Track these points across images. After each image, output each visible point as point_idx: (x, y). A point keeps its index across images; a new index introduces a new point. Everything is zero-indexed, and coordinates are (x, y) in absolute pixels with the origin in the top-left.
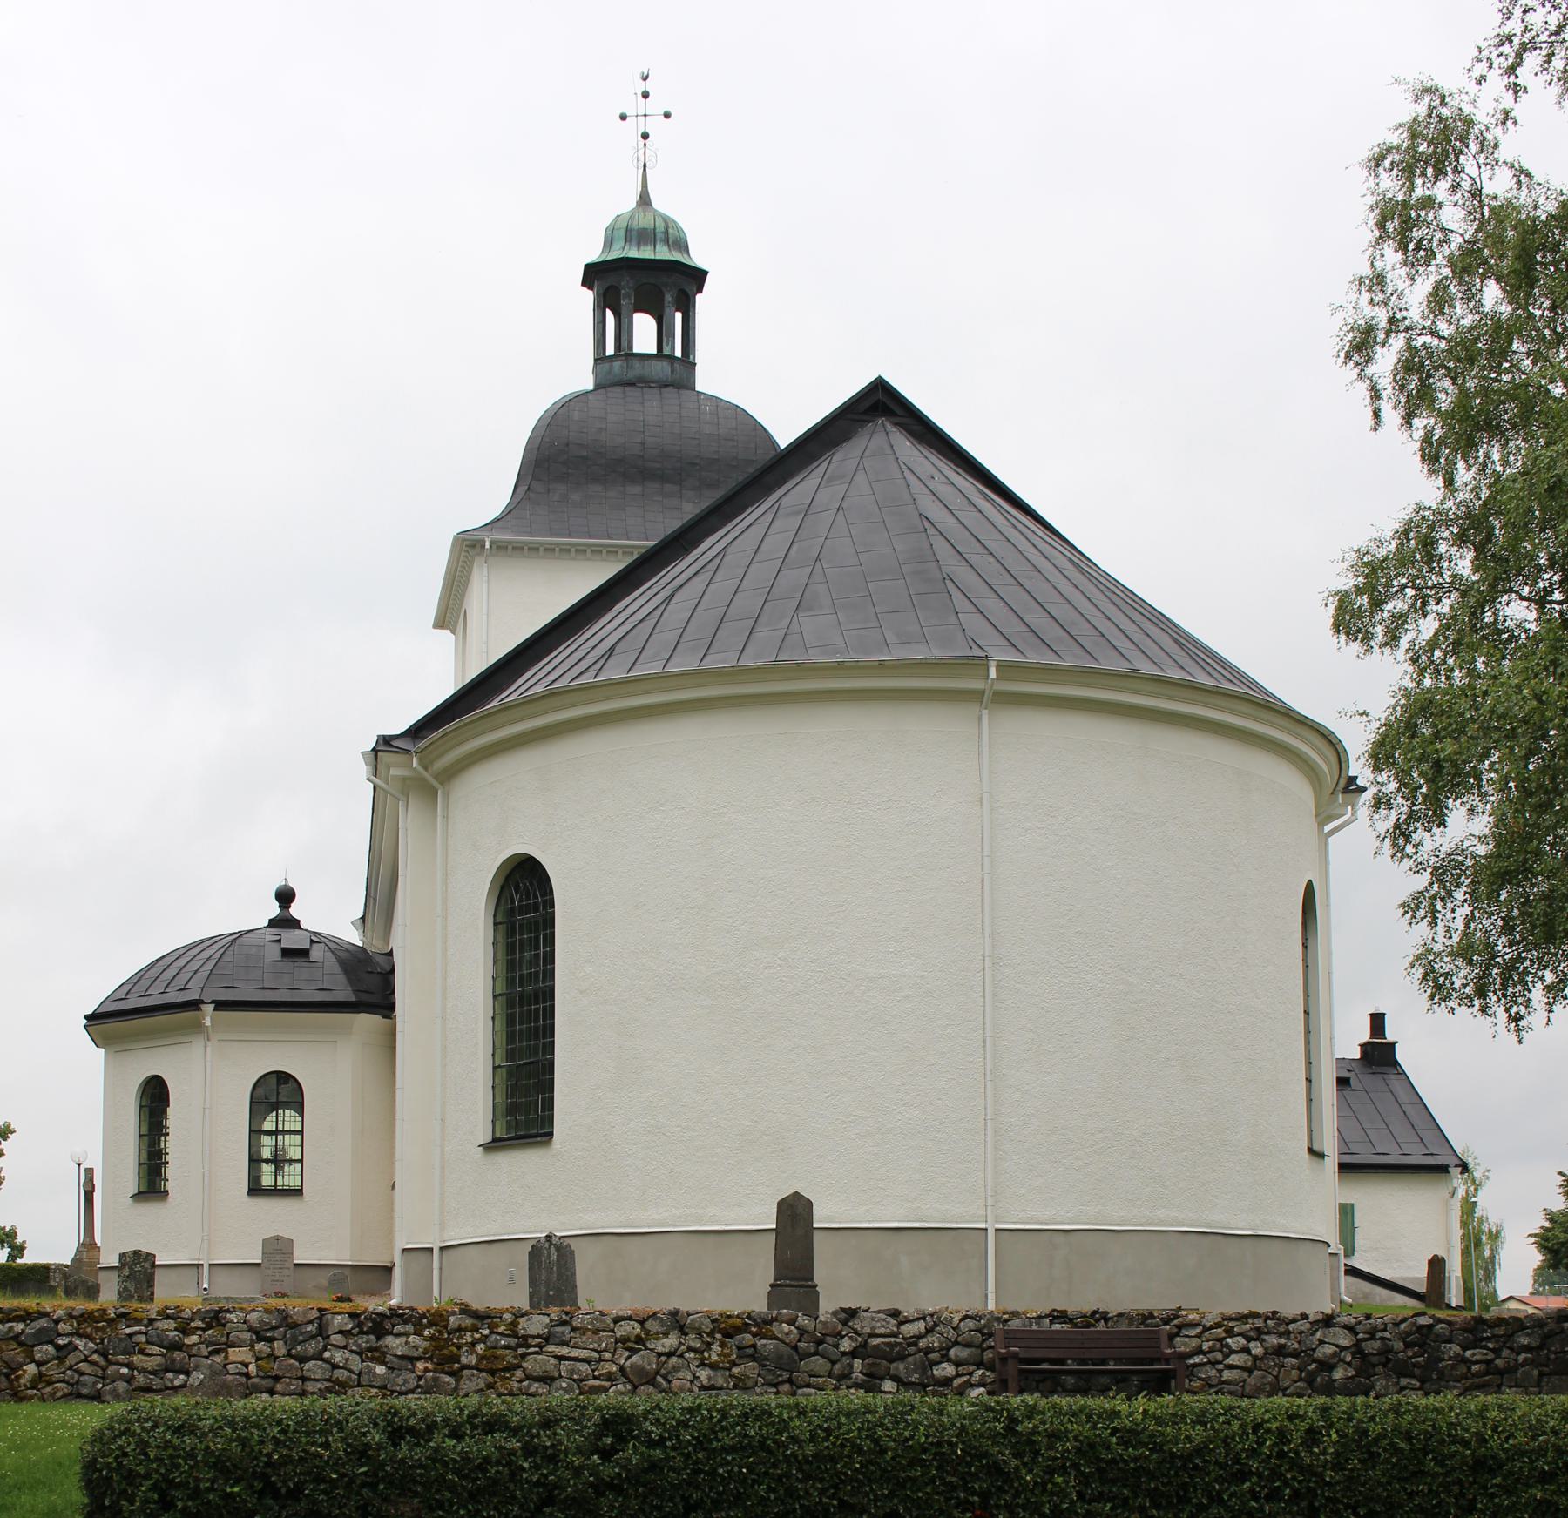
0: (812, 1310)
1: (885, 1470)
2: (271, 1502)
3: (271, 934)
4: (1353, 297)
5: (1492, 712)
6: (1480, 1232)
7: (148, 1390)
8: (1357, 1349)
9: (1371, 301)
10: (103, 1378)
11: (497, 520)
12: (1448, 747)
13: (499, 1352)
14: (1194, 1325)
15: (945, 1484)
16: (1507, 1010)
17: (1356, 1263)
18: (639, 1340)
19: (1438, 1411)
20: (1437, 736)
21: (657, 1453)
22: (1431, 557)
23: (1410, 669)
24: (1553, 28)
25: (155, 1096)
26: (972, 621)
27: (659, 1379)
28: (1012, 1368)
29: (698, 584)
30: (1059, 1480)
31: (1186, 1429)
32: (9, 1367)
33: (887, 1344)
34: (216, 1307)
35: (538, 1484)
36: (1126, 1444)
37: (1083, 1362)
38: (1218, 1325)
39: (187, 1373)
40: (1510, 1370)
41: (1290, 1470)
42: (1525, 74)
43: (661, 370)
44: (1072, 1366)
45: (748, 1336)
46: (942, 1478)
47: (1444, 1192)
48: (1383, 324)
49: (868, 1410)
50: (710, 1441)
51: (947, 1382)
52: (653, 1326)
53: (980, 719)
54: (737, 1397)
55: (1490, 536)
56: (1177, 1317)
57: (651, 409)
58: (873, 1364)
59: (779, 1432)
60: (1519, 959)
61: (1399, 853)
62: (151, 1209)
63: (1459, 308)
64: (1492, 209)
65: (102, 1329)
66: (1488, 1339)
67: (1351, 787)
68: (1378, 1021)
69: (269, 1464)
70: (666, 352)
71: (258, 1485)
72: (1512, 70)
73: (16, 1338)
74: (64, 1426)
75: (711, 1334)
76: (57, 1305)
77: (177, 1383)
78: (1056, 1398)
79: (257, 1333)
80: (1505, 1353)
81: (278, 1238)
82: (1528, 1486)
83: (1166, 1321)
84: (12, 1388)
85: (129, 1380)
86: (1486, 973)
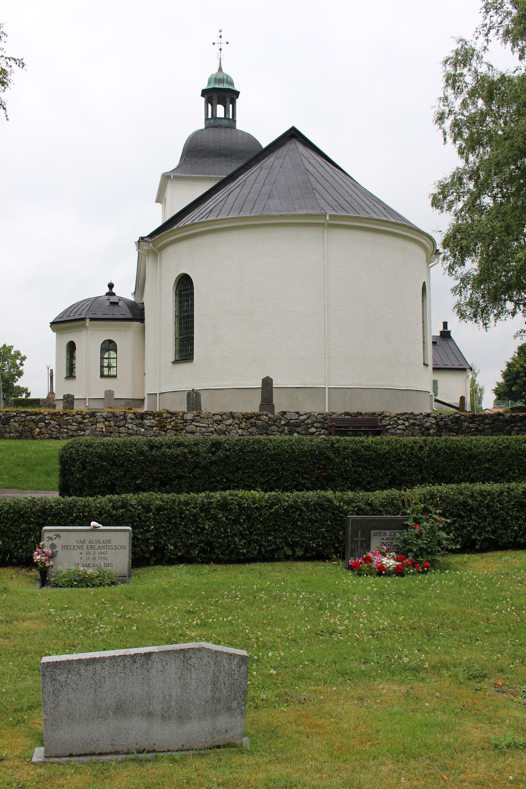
0: (273, 412)
1: (295, 458)
2: (115, 467)
3: (107, 297)
4: (438, 104)
5: (479, 232)
6: (477, 389)
7: (73, 436)
8: (437, 424)
9: (444, 105)
10: (59, 432)
11: (175, 169)
12: (464, 243)
13: (178, 424)
14: (387, 416)
15: (313, 462)
16: (483, 322)
17: (438, 398)
18: (220, 421)
19: (458, 441)
20: (462, 239)
21: (228, 453)
22: (461, 184)
23: (454, 218)
24: (499, 22)
25: (71, 347)
26: (322, 202)
27: (227, 433)
28: (333, 429)
29: (238, 190)
30: (346, 461)
31: (384, 446)
32: (31, 429)
33: (295, 422)
34: (93, 411)
35: (193, 462)
36: (366, 450)
37: (354, 427)
38: (395, 417)
39: (85, 431)
40: (483, 430)
41: (414, 458)
42: (490, 36)
43: (226, 122)
44: (351, 429)
45: (253, 420)
46: (312, 461)
47: (465, 377)
48: (447, 112)
49: (290, 440)
50: (244, 450)
51: (313, 434)
52: (225, 417)
53: (324, 232)
54: (251, 437)
55: (479, 177)
56: (383, 414)
57: (222, 135)
58: (291, 428)
59: (264, 447)
60: (487, 306)
61: (450, 274)
62: (70, 382)
63: (470, 107)
64: (481, 77)
65: (59, 418)
66: (476, 421)
67: (437, 253)
68: (445, 324)
69: (114, 456)
70: (227, 117)
71: (111, 463)
72: (486, 35)
73: (33, 420)
74: (49, 447)
75: (242, 419)
76: (45, 410)
77: (81, 434)
78: (346, 437)
79: (105, 419)
80: (482, 425)
81: (109, 391)
82: (484, 463)
83: (380, 415)
84: (32, 435)
85: (67, 433)
86: (477, 310)
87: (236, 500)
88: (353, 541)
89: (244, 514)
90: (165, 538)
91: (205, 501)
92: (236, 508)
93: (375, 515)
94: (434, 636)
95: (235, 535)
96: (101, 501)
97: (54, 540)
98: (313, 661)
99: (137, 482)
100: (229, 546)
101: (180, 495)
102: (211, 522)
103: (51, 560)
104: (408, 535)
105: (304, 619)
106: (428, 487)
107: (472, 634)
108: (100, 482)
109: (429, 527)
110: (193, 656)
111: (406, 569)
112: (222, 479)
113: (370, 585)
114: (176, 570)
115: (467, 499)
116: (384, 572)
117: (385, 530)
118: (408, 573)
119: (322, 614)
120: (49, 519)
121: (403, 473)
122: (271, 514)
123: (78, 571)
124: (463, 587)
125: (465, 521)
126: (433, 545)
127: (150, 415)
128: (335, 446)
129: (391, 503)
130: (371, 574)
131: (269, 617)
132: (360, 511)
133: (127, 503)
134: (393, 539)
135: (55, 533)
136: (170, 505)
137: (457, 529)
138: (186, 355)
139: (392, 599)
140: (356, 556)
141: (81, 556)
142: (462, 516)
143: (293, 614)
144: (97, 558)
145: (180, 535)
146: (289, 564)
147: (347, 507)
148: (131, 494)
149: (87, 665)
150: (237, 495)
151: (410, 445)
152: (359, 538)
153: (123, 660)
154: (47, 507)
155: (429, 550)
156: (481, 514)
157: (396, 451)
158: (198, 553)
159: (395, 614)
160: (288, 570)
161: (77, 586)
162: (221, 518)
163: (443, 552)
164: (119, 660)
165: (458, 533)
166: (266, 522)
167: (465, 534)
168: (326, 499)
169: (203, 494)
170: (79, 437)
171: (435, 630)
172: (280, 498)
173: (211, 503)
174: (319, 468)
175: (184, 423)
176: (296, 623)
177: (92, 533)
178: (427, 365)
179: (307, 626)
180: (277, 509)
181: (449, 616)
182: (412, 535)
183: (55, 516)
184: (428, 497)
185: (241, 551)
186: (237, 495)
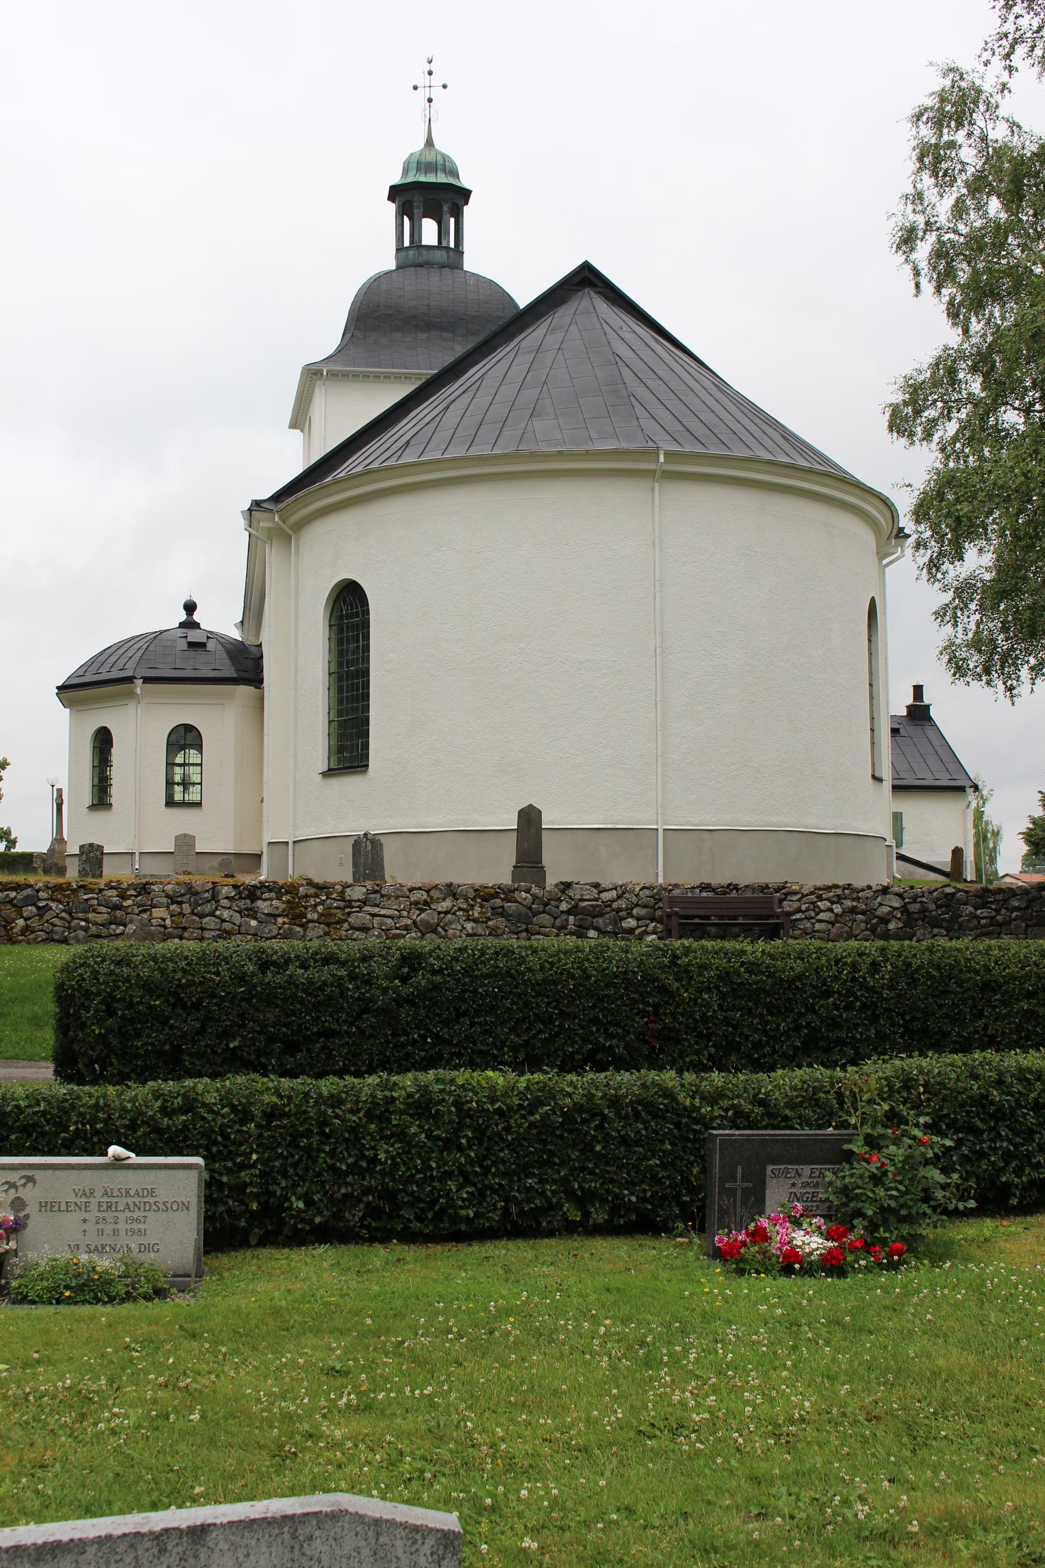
0: (541, 883)
3: (181, 632)
4: (902, 208)
6: (986, 831)
7: (99, 936)
8: (904, 910)
10: (69, 928)
11: (331, 356)
12: (965, 508)
13: (333, 911)
14: (795, 893)
15: (630, 999)
16: (1004, 683)
18: (426, 903)
19: (959, 950)
20: (958, 500)
21: (438, 978)
22: (953, 381)
23: (940, 456)
24: (1035, 28)
25: (103, 740)
26: (648, 424)
27: (439, 929)
28: (674, 922)
29: (465, 399)
30: (706, 996)
31: (790, 962)
32: (6, 921)
33: (591, 906)
34: (144, 881)
35: (358, 999)
36: (750, 972)
37: (722, 918)
38: (812, 893)
39: (125, 925)
40: (1006, 923)
41: (860, 990)
42: (1016, 59)
43: (440, 256)
44: (714, 920)
46: (628, 995)
47: (962, 804)
48: (922, 226)
50: (473, 971)
51: (631, 931)
52: (435, 894)
53: (653, 489)
55: (993, 367)
56: (784, 888)
57: (434, 282)
59: (519, 965)
61: (932, 578)
62: (100, 816)
63: (973, 215)
64: (994, 149)
65: (68, 896)
66: (991, 902)
67: (901, 534)
68: (918, 691)
69: (179, 986)
70: (444, 244)
71: (172, 1000)
72: (1007, 56)
73: (11, 902)
74: (42, 961)
75: (474, 899)
76: (38, 879)
77: (118, 932)
78: (704, 942)
79: (171, 898)
80: (1003, 911)
81: (185, 835)
82: (1018, 1000)
83: (777, 890)
84: (7, 934)
85: (86, 929)
86: (990, 659)
87: (450, 1093)
88: (723, 1190)
89: (469, 1127)
90: (283, 1183)
91: (379, 1095)
92: (450, 1112)
93: (774, 1128)
94: (927, 1438)
95: (449, 1175)
96: (136, 1095)
97: (20, 1189)
98: (629, 1510)
99: (232, 1045)
100: (434, 1202)
101: (322, 1082)
102: (392, 1145)
103: (13, 1236)
104: (852, 1175)
105: (608, 1393)
106: (897, 1062)
107: (1020, 1434)
108: (147, 1044)
109: (901, 1159)
110: (317, 1533)
111: (850, 1258)
112: (424, 1037)
113: (765, 1299)
114: (308, 1260)
115: (988, 1091)
116: (797, 1266)
117: (798, 1164)
118: (853, 1268)
119: (651, 1378)
120: (13, 1137)
121: (834, 1024)
122: (532, 1125)
123: (76, 1264)
124: (986, 1305)
125: (984, 1142)
126: (911, 1200)
127: (270, 890)
128: (679, 962)
129: (811, 1099)
130: (767, 1272)
131: (525, 1387)
132: (739, 1119)
133: (195, 1100)
134: (816, 1186)
135: (24, 1173)
136: (296, 1105)
137: (965, 1159)
138: (351, 757)
139: (818, 1335)
140: (732, 1226)
141: (85, 1226)
142: (978, 1128)
143: (581, 1379)
144: (122, 1233)
145: (319, 1174)
146: (574, 1243)
147: (709, 1109)
148: (207, 1080)
149: (38, 1560)
150: (452, 1081)
151: (849, 960)
152: (739, 1184)
153: (132, 1546)
154: (9, 1109)
155: (903, 1212)
156: (1021, 1124)
157: (818, 973)
158: (363, 1218)
159: (828, 1377)
160: (572, 1259)
161: (71, 1301)
162: (415, 1135)
163: (935, 1218)
164: (122, 1547)
165: (969, 1168)
166: (521, 1145)
167: (985, 1171)
168: (660, 1089)
169: (373, 1080)
170: (99, 941)
171: (927, 1421)
172: (551, 1089)
173: (393, 1099)
174: (643, 1013)
175: (346, 907)
176: (590, 1404)
177: (111, 1172)
178: (880, 780)
179: (616, 1412)
180: (546, 1113)
181: (958, 1382)
182: (861, 1177)
183: (26, 1130)
184: (898, 1085)
185: (463, 1212)
186: (452, 1081)
